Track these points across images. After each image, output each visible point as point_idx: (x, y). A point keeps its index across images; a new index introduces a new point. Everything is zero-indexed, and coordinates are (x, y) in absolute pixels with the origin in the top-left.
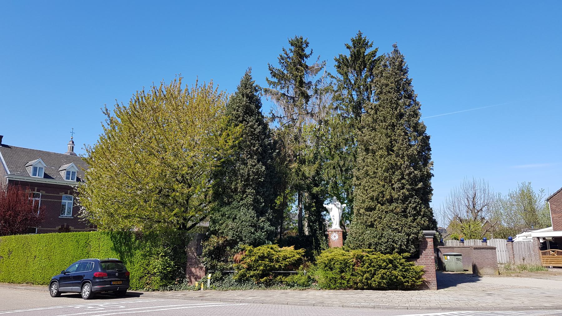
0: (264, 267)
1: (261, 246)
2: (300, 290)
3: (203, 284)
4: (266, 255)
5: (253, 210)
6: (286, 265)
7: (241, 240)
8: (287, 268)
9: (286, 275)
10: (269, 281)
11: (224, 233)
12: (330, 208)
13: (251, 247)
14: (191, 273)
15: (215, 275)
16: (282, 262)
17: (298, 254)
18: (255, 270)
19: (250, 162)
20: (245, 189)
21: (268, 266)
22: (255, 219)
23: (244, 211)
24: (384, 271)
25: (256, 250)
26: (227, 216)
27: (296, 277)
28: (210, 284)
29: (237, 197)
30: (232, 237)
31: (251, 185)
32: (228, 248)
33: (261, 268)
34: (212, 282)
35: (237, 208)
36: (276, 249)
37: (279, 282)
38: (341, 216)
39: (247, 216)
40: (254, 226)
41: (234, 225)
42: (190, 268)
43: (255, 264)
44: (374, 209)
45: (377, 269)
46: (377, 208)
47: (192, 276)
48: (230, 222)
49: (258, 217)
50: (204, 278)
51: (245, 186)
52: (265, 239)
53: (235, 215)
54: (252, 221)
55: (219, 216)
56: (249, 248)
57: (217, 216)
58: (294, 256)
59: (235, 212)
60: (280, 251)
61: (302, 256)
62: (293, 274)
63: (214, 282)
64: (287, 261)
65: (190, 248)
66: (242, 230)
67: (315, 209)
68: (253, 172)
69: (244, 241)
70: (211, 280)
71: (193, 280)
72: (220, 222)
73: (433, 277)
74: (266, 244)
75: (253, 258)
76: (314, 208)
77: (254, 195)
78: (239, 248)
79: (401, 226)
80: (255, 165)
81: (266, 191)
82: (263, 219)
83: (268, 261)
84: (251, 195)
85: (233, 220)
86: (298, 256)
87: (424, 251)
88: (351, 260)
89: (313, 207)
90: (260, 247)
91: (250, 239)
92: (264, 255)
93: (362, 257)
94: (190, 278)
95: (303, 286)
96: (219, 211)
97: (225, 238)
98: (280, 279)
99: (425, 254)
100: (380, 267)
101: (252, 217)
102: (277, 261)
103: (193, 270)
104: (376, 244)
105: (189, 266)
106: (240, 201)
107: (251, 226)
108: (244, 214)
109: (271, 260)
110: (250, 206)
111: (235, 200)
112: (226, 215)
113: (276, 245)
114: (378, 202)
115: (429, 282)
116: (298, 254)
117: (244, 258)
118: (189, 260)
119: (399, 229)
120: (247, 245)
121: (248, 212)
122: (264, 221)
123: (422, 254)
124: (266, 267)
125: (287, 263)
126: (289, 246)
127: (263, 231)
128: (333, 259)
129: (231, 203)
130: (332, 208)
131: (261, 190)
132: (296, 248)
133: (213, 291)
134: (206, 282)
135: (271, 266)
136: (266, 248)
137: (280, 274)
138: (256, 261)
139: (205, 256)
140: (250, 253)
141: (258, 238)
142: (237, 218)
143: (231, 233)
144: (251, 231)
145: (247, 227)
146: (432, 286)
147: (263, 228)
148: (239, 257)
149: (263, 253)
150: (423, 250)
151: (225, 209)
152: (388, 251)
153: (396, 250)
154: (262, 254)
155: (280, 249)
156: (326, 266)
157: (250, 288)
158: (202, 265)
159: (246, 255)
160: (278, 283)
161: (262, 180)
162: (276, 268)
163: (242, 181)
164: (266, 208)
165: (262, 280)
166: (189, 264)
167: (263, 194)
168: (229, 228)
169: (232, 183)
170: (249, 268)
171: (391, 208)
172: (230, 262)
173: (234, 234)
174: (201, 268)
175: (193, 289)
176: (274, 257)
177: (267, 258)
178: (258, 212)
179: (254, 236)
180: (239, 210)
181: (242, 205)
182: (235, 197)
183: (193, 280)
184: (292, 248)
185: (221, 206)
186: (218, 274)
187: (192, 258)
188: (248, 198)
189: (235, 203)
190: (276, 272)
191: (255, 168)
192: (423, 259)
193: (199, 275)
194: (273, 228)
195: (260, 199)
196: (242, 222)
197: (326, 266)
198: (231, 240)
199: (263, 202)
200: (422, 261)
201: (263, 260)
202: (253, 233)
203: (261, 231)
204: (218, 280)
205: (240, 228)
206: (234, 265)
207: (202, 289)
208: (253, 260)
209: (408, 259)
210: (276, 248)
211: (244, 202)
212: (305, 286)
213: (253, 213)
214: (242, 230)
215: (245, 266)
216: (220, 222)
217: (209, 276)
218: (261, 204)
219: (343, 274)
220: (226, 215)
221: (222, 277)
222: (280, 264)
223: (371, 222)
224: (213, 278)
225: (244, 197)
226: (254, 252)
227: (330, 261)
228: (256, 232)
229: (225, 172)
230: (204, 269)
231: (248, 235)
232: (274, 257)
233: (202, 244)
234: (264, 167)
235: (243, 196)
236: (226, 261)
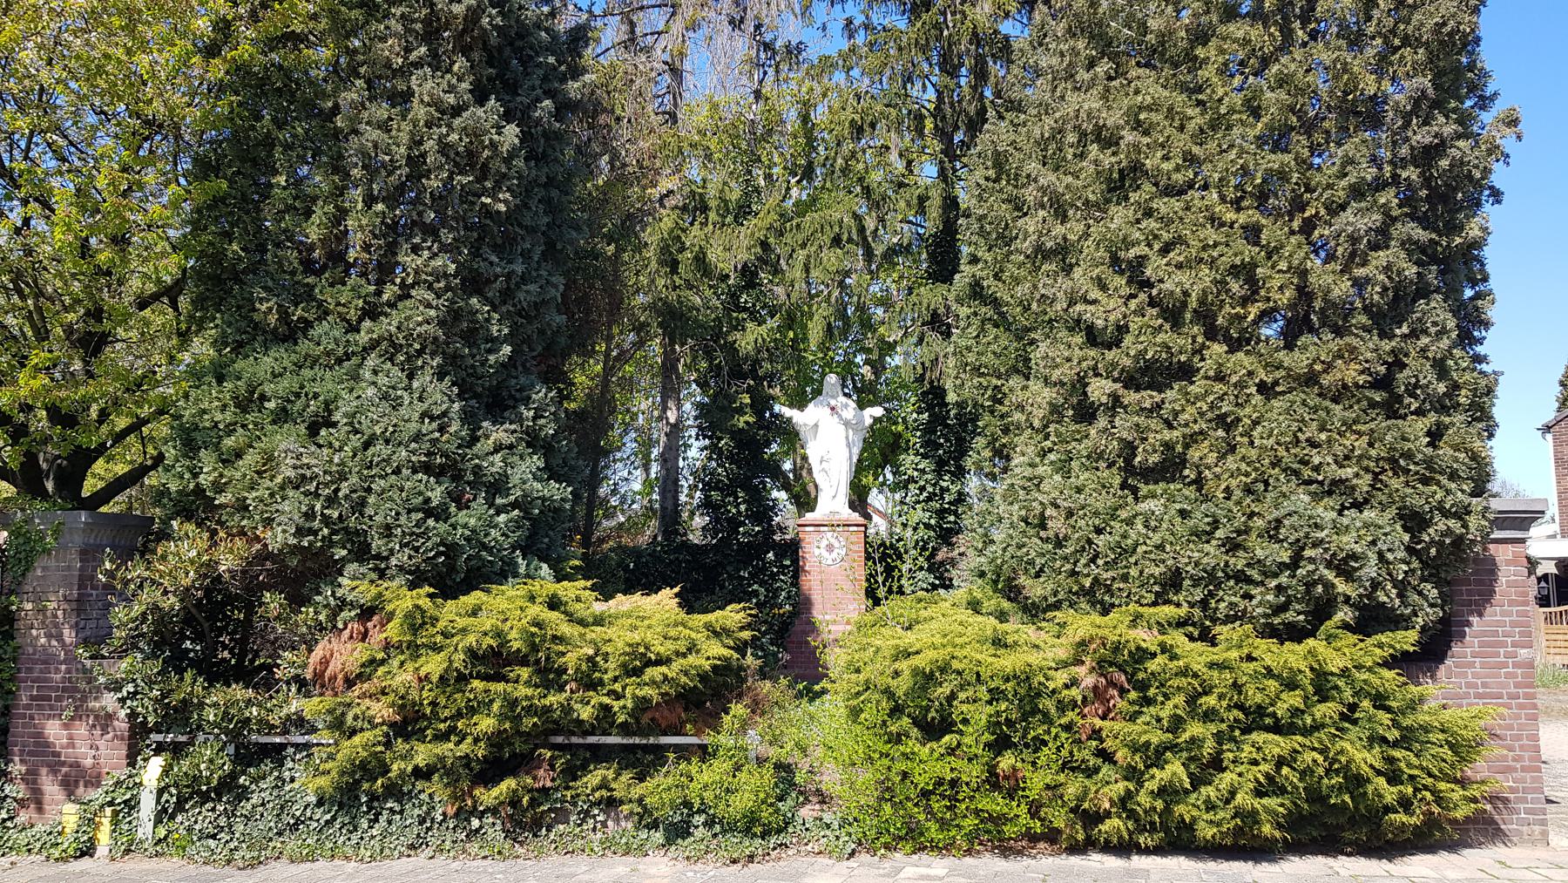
0: (502, 717)
1: (488, 591)
2: (734, 862)
3: (106, 822)
4: (516, 645)
5: (441, 379)
6: (642, 704)
7: (361, 552)
8: (645, 720)
9: (643, 761)
10: (534, 803)
11: (246, 508)
12: (812, 423)
13: (421, 597)
14: (43, 753)
15: (185, 764)
16: (617, 687)
17: (716, 633)
18: (442, 737)
19: (424, 85)
20: (392, 249)
21: (530, 710)
22: (452, 429)
23: (382, 380)
24: (1278, 745)
25: (451, 612)
26: (271, 405)
27: (707, 775)
28: (158, 821)
29: (347, 296)
30: (300, 532)
31: (431, 231)
32: (273, 602)
33: (486, 724)
34: (165, 810)
35: (339, 361)
36: (578, 606)
37: (593, 805)
38: (855, 460)
39: (402, 411)
40: (446, 468)
41: (316, 460)
42: (32, 718)
43: (442, 701)
44: (1186, 372)
45: (1232, 728)
46: (1208, 366)
47: (44, 771)
48: (286, 441)
49: (469, 418)
50: (118, 783)
51: (392, 235)
52: (514, 548)
53: (327, 403)
54: (434, 442)
55: (224, 408)
56: (404, 599)
57: (213, 404)
58: (690, 650)
59: (327, 383)
60: (599, 621)
61: (741, 648)
62: (684, 752)
63: (180, 807)
64: (653, 683)
65: (38, 599)
66: (369, 490)
67: (751, 420)
68: (444, 148)
69: (378, 557)
70: (160, 792)
71: (51, 789)
72: (229, 442)
73: (1523, 769)
74: (516, 575)
75: (433, 665)
76: (747, 418)
77: (448, 288)
78: (343, 604)
79: (1367, 470)
80: (457, 111)
81: (524, 279)
82: (499, 434)
83: (528, 683)
84: (430, 287)
85: (313, 430)
86: (716, 649)
87: (1474, 619)
88: (1061, 677)
89: (740, 411)
90: (478, 593)
91: (416, 549)
92: (501, 645)
93: (1142, 655)
94: (31, 779)
95: (747, 831)
96: (220, 379)
97: (258, 539)
98: (604, 785)
99: (1484, 634)
100: (1257, 718)
101: (432, 419)
102: (590, 683)
103: (54, 730)
104: (1211, 579)
105: (28, 707)
106: (360, 320)
107: (427, 468)
108: (385, 397)
109: (550, 676)
110: (420, 353)
111: (327, 313)
112: (263, 398)
113: (582, 583)
114: (1212, 333)
115: (1506, 801)
116: (716, 633)
117: (373, 663)
118: (30, 670)
119: (1353, 488)
120: (395, 583)
121: (408, 388)
122: (511, 447)
123: (1463, 635)
124: (517, 719)
125: (647, 691)
126: (651, 588)
127: (499, 501)
128: (943, 670)
129: (305, 333)
130: (816, 425)
131: (494, 265)
132: (690, 603)
133: (172, 864)
134: (132, 805)
135: (548, 710)
136: (520, 603)
137: (600, 755)
138: (453, 681)
139: (135, 646)
140: (415, 629)
141: (468, 539)
142: (337, 417)
143: (291, 507)
144: (427, 501)
145: (397, 471)
146: (1522, 822)
147: (498, 486)
148: (343, 654)
149: (499, 634)
150: (1471, 613)
151: (263, 364)
152: (1290, 616)
153: (1344, 614)
154: (489, 641)
155: (599, 607)
156: (896, 711)
157: (412, 847)
158: (109, 701)
159: (387, 646)
160: (587, 813)
161: (502, 208)
162: (579, 722)
163: (370, 200)
164: (523, 380)
165: (489, 796)
166: (32, 698)
167: (507, 294)
168: (279, 479)
169: (308, 213)
170: (409, 724)
171: (1298, 360)
172: (288, 683)
173: (309, 515)
174: (104, 721)
175: (48, 846)
176: (571, 660)
177: (524, 662)
178: (476, 396)
179: (442, 527)
180: (356, 377)
181: (374, 345)
182: (328, 296)
183: (51, 789)
184: (665, 601)
185: (238, 348)
186: (208, 758)
187: (48, 660)
188: (408, 303)
189: (327, 333)
190: (575, 740)
191: (457, 122)
192: (1472, 665)
193: (88, 762)
194: (557, 491)
195: (487, 320)
196: (367, 445)
197: (896, 711)
198: (296, 549)
199: (506, 340)
200: (1465, 675)
201: (499, 678)
202: (440, 514)
203: (491, 505)
204: (205, 798)
205: (354, 479)
206: (309, 707)
207: (102, 850)
208: (435, 678)
209: (1407, 663)
210: (578, 599)
211: (388, 325)
212: (758, 830)
213: (438, 393)
214: (369, 490)
215: (382, 710)
216: (229, 442)
217: (153, 770)
218: (497, 351)
219: (1006, 762)
220: (263, 398)
221: (233, 776)
222: (606, 700)
223: (1168, 446)
224: (176, 785)
225: (385, 297)
226: (441, 625)
227: (926, 679)
228: (460, 509)
229: (269, 142)
230: (122, 725)
231: (403, 519)
232: (571, 660)
233: (110, 574)
234: (512, 132)
235: (379, 293)
236: (261, 679)
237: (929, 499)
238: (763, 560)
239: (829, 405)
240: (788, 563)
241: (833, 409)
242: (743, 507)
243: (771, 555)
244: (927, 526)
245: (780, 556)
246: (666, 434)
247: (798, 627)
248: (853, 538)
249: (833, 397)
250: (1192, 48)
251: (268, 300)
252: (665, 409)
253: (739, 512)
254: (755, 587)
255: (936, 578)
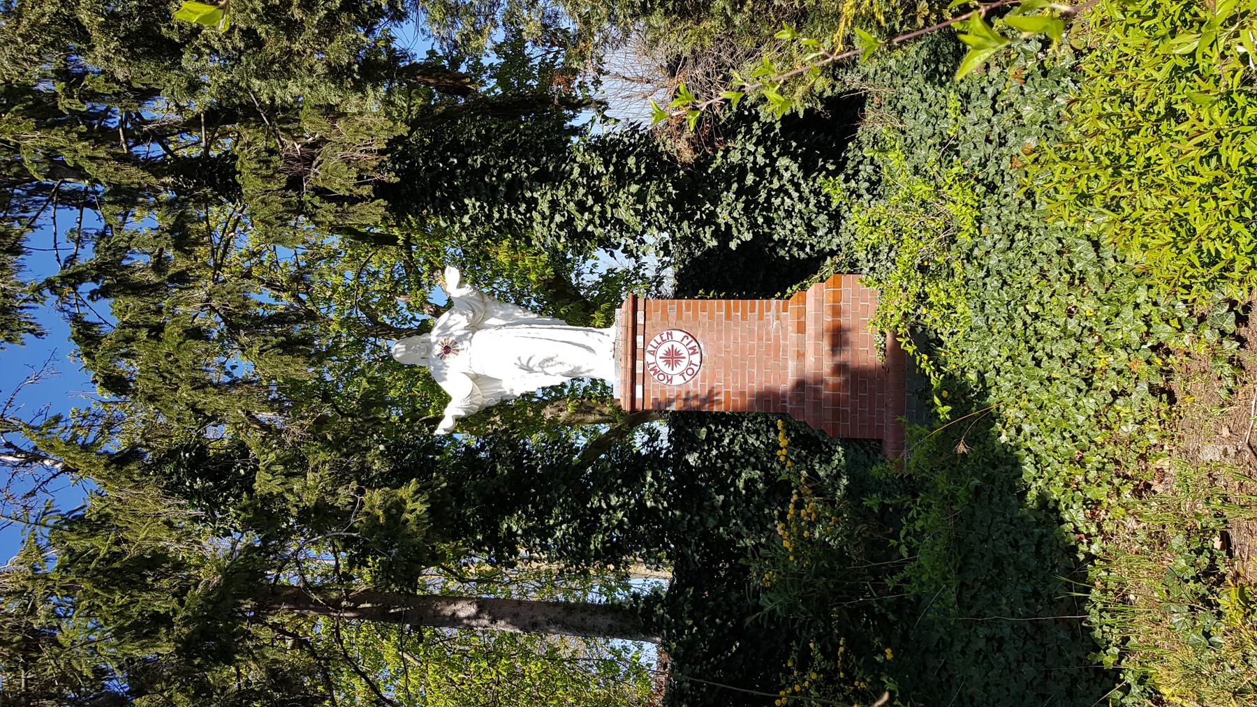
237: (599, 198)
238: (699, 470)
239: (441, 357)
240: (703, 432)
241: (447, 349)
242: (614, 500)
243: (692, 459)
244: (641, 197)
245: (692, 444)
246: (493, 621)
247: (808, 416)
248: (656, 317)
249: (429, 349)
250: (860, 504)
251: (600, 688)
252: (454, 621)
253: (623, 506)
254: (741, 484)
255: (728, 189)
